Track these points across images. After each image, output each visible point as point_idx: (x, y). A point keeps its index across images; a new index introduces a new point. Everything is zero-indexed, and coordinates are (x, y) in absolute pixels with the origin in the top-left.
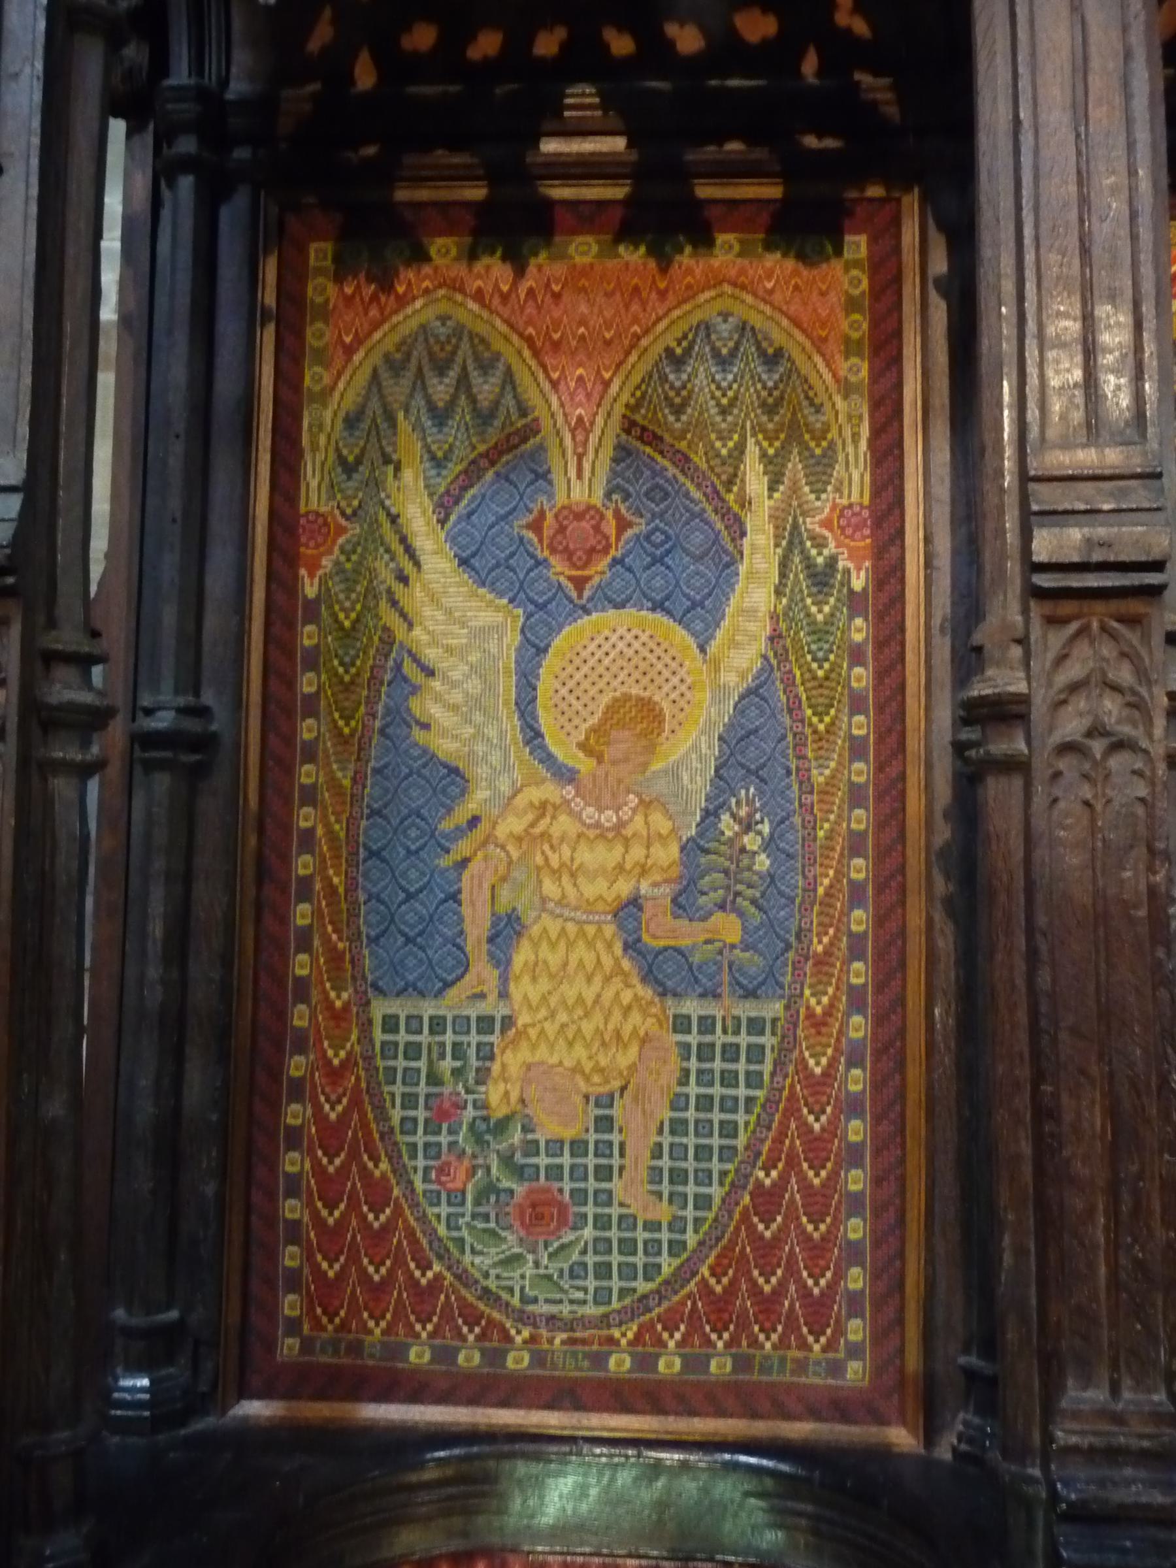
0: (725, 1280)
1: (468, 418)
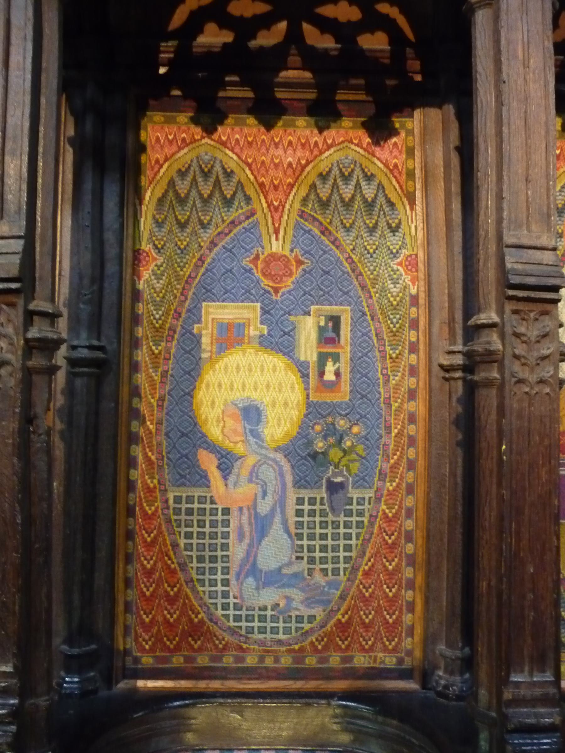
0: (394, 617)
1: (220, 203)
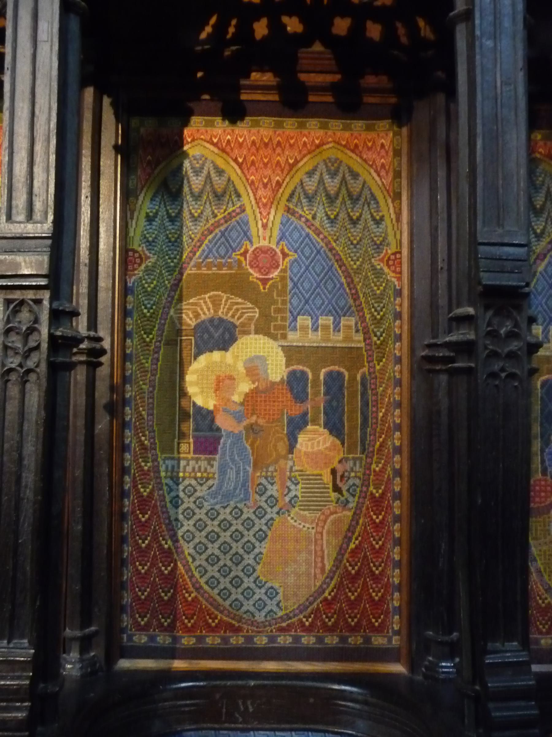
1: (324, 199)
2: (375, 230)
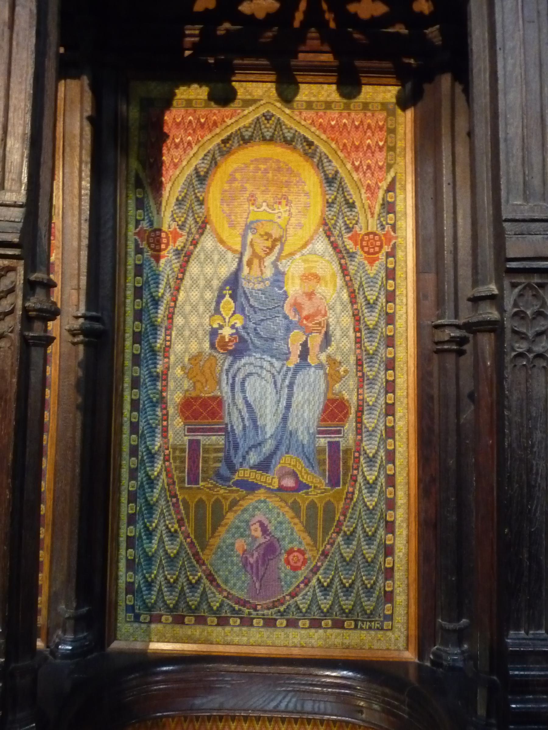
2: (198, 211)
